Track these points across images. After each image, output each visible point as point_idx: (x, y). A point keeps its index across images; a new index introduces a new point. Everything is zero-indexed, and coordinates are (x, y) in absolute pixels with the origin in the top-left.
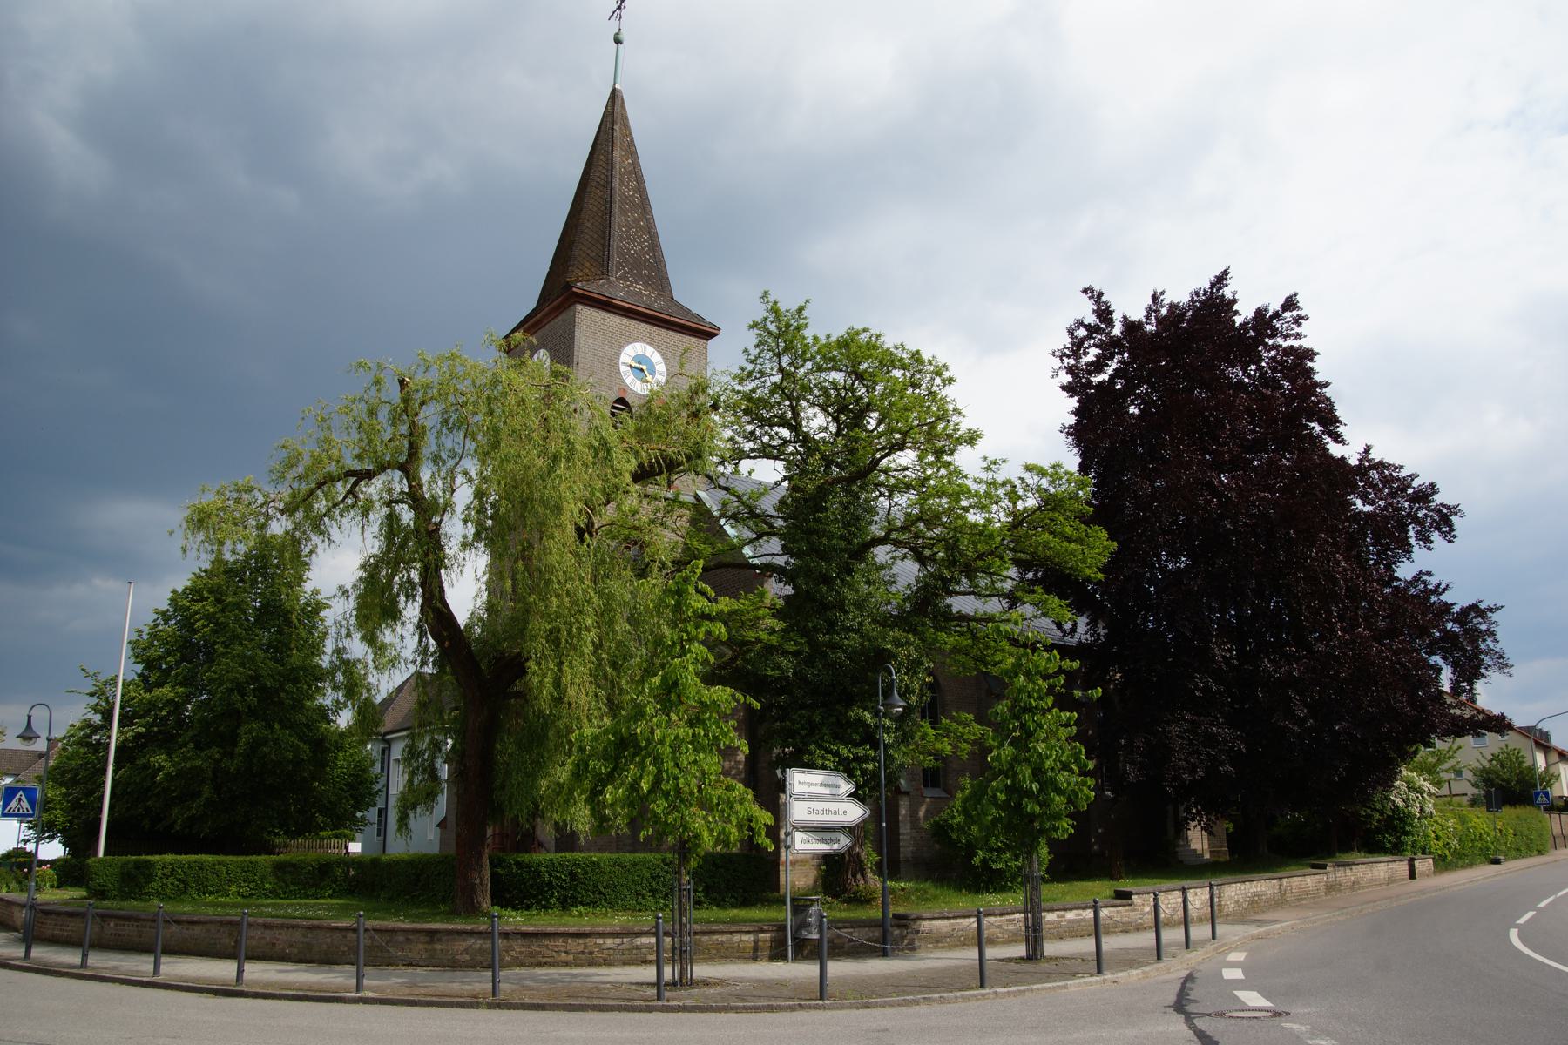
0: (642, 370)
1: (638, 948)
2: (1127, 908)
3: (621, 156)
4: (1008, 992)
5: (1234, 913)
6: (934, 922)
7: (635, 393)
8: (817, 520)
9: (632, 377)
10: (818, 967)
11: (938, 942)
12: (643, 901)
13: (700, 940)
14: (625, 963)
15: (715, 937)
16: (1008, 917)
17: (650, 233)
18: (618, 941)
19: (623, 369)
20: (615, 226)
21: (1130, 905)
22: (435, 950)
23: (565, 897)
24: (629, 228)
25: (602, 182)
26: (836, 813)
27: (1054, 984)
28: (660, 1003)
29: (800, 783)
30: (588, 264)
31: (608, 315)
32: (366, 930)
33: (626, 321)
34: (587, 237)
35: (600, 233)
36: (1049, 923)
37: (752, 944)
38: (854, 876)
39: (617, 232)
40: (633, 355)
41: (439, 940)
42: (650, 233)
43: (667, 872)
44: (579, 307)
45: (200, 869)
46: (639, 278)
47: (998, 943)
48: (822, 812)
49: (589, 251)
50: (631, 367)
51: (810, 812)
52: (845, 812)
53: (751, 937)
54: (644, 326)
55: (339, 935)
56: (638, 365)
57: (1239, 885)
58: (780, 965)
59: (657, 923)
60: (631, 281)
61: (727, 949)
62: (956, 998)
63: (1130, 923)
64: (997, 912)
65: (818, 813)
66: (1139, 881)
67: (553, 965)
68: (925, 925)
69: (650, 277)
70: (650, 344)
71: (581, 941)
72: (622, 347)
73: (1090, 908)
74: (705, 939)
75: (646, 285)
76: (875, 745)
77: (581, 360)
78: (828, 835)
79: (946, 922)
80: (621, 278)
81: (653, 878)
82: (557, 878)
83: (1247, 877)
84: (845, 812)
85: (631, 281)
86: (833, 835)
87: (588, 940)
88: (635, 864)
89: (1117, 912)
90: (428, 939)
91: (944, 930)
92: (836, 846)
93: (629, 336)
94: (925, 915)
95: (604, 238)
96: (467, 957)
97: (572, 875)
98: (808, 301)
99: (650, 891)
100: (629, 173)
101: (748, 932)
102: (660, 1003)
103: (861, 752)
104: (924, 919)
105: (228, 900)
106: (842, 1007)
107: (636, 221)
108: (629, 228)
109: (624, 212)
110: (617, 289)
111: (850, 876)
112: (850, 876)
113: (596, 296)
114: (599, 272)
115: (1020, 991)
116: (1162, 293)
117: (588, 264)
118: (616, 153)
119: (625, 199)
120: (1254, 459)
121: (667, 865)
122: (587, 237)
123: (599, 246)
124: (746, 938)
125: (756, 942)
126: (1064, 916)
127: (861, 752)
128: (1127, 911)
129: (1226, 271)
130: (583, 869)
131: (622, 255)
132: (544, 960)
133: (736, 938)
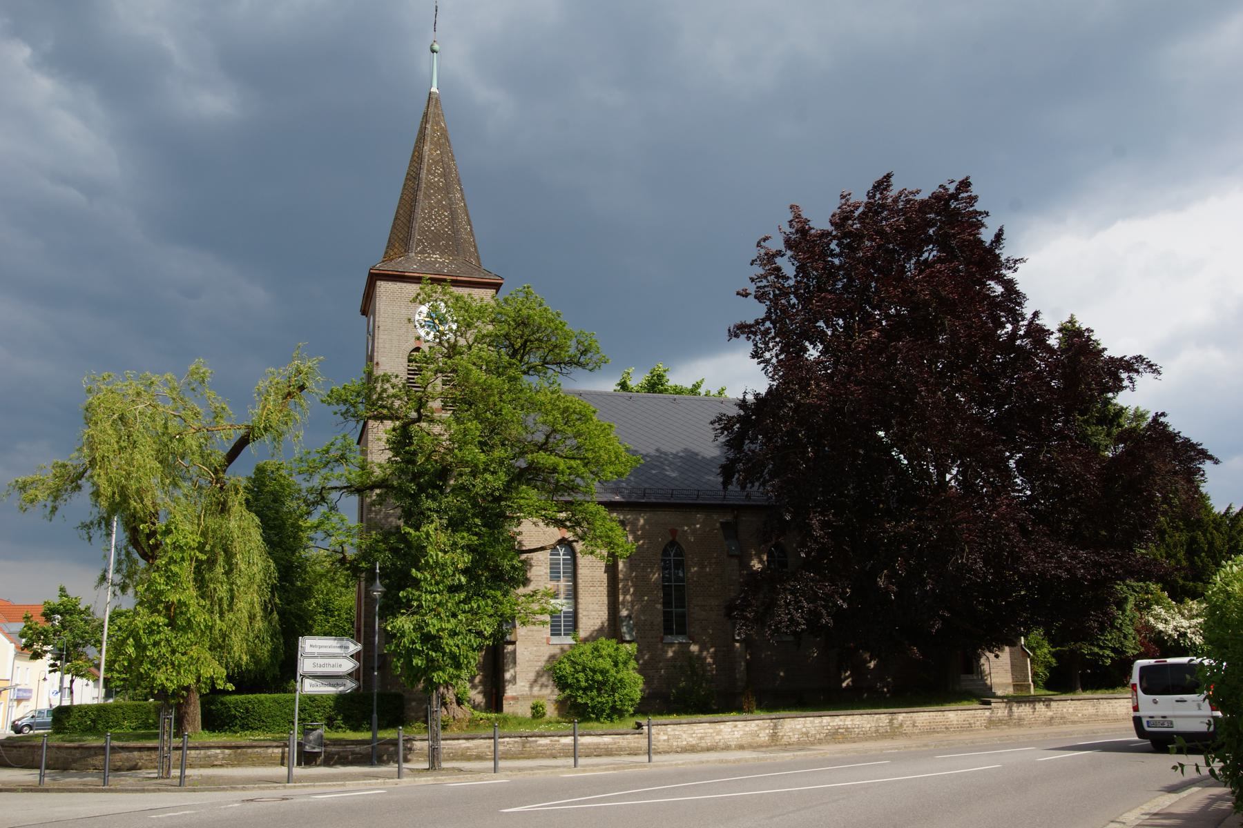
1: (209, 757)
2: (637, 736)
3: (430, 150)
5: (799, 743)
14: (202, 766)
17: (450, 209)
18: (198, 752)
23: (243, 724)
29: (311, 646)
31: (405, 284)
36: (582, 744)
42: (450, 209)
44: (378, 283)
51: (315, 665)
53: (280, 750)
73: (571, 735)
74: (250, 750)
75: (442, 255)
77: (380, 324)
78: (334, 681)
80: (420, 252)
83: (849, 712)
84: (340, 666)
85: (429, 254)
86: (340, 681)
89: (624, 739)
91: (788, 759)
92: (341, 689)
95: (409, 222)
97: (247, 709)
100: (436, 163)
101: (277, 747)
105: (122, 731)
107: (440, 201)
109: (428, 197)
113: (390, 273)
114: (403, 251)
119: (430, 185)
120: (1003, 316)
121: (313, 701)
124: (276, 750)
125: (283, 753)
126: (558, 741)
128: (638, 738)
130: (253, 705)
131: (423, 233)
133: (270, 750)
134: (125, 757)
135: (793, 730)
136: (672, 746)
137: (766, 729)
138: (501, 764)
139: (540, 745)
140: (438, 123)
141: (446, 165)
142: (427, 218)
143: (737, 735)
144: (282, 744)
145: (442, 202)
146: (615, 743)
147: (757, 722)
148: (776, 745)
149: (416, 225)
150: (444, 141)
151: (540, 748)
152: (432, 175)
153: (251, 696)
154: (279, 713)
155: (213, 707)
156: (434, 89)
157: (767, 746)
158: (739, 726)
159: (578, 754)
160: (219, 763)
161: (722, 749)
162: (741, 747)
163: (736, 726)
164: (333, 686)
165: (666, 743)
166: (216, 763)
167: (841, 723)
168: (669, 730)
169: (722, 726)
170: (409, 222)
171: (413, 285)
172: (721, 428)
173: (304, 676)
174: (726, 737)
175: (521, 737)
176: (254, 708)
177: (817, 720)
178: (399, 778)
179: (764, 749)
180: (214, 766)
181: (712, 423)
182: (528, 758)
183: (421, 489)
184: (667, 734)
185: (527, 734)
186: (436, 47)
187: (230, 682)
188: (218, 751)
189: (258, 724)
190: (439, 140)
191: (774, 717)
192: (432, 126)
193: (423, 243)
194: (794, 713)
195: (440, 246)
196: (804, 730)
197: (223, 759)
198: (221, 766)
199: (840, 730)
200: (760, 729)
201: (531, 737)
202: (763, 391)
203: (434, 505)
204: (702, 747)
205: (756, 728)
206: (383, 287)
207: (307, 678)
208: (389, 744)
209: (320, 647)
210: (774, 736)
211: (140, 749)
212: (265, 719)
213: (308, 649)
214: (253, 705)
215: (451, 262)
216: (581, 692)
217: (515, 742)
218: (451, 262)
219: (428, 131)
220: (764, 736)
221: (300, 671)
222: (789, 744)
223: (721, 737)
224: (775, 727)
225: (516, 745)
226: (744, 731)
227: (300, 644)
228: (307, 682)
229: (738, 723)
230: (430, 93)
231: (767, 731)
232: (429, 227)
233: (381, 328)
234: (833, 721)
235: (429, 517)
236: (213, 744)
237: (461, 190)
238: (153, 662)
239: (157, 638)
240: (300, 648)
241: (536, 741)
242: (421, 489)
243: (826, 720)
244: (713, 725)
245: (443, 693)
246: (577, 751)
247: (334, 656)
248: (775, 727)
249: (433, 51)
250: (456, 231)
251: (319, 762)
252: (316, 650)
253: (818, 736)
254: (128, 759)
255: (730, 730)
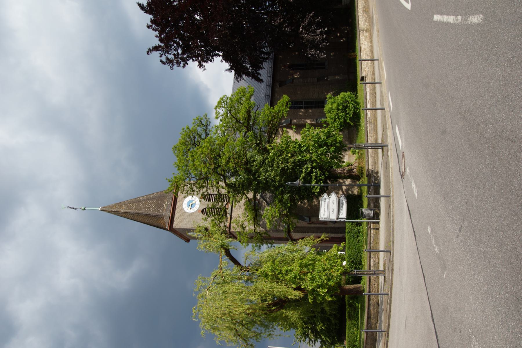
0: (192, 205)
1: (374, 265)
2: (366, 79)
4: (392, 191)
5: (369, 23)
6: (369, 164)
7: (200, 207)
8: (239, 186)
9: (194, 208)
10: (382, 198)
11: (376, 163)
12: (361, 241)
13: (372, 247)
15: (372, 242)
16: (368, 133)
17: (146, 200)
19: (192, 211)
20: (146, 213)
21: (366, 77)
22: (373, 317)
23: (359, 264)
24: (146, 208)
25: (132, 215)
26: (334, 204)
27: (391, 172)
28: (389, 294)
30: (159, 222)
31: (175, 216)
32: (367, 329)
33: (176, 210)
34: (150, 221)
35: (149, 217)
36: (371, 106)
37: (374, 230)
38: (354, 172)
39: (148, 212)
40: (187, 208)
41: (370, 316)
42: (146, 200)
43: (352, 232)
44: (174, 227)
45: (350, 342)
46: (162, 205)
47: (377, 138)
48: (333, 208)
49: (155, 221)
50: (191, 208)
52: (333, 200)
53: (372, 230)
54: (178, 204)
55: (368, 338)
56: (190, 206)
57: (359, 19)
58: (380, 229)
59: (367, 251)
60: (164, 208)
61: (375, 238)
62: (393, 211)
63: (372, 77)
64: (367, 139)
65: (333, 210)
66: (358, 75)
67: (378, 288)
68: (370, 168)
69: (161, 201)
70: (183, 202)
71: (371, 281)
72: (185, 212)
74: (372, 245)
75: (164, 202)
76: (311, 172)
77: (191, 227)
79: (369, 159)
81: (354, 237)
82: (353, 266)
84: (333, 200)
85: (164, 208)
86: (341, 202)
87: (371, 279)
88: (349, 243)
90: (370, 319)
93: (181, 209)
94: (367, 168)
95: (150, 216)
96: (375, 310)
97: (352, 262)
98: (166, 179)
99: (357, 238)
100: (128, 206)
101: (370, 231)
102: (389, 294)
103: (314, 177)
104: (368, 168)
106: (393, 249)
107: (143, 204)
108: (146, 208)
109: (141, 209)
110: (167, 214)
111: (354, 174)
112: (354, 174)
113: (170, 222)
115: (392, 187)
116: (148, 25)
117: (159, 222)
118: (122, 211)
119: (136, 208)
121: (349, 232)
122: (150, 221)
123: (153, 218)
125: (373, 229)
126: (369, 118)
127: (314, 177)
129: (138, 4)
130: (350, 259)
132: (377, 290)
133: (372, 235)
134: (372, 307)
135: (364, 24)
136: (371, 66)
137: (363, 34)
138: (378, 106)
139: (371, 116)
140: (113, 207)
141: (127, 203)
142: (149, 209)
143: (366, 43)
144: (369, 229)
145: (143, 204)
146: (370, 87)
147: (360, 36)
148: (370, 30)
149: (152, 213)
150: (120, 204)
151: (372, 116)
152: (132, 208)
153: (347, 327)
154: (354, 247)
155: (351, 280)
156: (99, 209)
157: (371, 33)
158: (362, 42)
159: (374, 82)
160: (377, 260)
161: (372, 48)
162: (371, 42)
163: (362, 43)
164: (343, 205)
165: (370, 68)
166: (377, 261)
167: (361, 9)
168: (364, 67)
169: (362, 48)
170: (150, 216)
171: (176, 213)
172: (240, 78)
173: (338, 218)
174: (367, 47)
175: (367, 124)
176: (351, 258)
177: (360, 17)
178: (388, 146)
179: (372, 34)
180: (378, 262)
181: (238, 82)
182: (376, 121)
183: (255, 179)
184: (366, 68)
185: (366, 121)
186: (83, 208)
187: (340, 244)
188: (372, 260)
189: (359, 256)
190: (119, 206)
191: (358, 31)
192: (114, 209)
193: (159, 210)
194: (357, 25)
195: (161, 204)
196: (364, 21)
197: (375, 258)
198: (378, 259)
199: (364, 10)
200: (364, 35)
201: (367, 120)
202: (226, 65)
203: (263, 174)
204: (371, 55)
205: (363, 37)
206: (176, 225)
207: (339, 217)
208: (370, 180)
209: (325, 211)
210: (366, 31)
211: (369, 300)
212: (357, 253)
213: (325, 216)
214: (350, 259)
215: (168, 199)
216: (347, 115)
217: (369, 126)
218: (168, 199)
219: (115, 210)
220: (367, 34)
221: (335, 220)
222: (370, 26)
223: (367, 49)
224: (363, 30)
225: (371, 126)
226: (364, 41)
227: (323, 220)
228: (341, 216)
229: (361, 43)
230: (101, 210)
231: (364, 33)
232: (153, 208)
233: (192, 226)
234: (360, 12)
235: (268, 176)
236: (368, 263)
237: (140, 197)
238: (329, 280)
239: (317, 277)
240: (325, 220)
241: (369, 118)
242: (255, 179)
243: (359, 14)
244: (362, 51)
245: (347, 171)
246: (372, 82)
247: (329, 202)
248: (363, 30)
249: (85, 209)
250: (155, 197)
251: (378, 212)
252: (326, 213)
253: (367, 17)
254: (373, 306)
255: (364, 46)
